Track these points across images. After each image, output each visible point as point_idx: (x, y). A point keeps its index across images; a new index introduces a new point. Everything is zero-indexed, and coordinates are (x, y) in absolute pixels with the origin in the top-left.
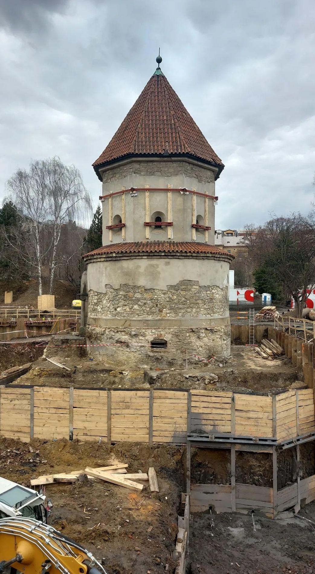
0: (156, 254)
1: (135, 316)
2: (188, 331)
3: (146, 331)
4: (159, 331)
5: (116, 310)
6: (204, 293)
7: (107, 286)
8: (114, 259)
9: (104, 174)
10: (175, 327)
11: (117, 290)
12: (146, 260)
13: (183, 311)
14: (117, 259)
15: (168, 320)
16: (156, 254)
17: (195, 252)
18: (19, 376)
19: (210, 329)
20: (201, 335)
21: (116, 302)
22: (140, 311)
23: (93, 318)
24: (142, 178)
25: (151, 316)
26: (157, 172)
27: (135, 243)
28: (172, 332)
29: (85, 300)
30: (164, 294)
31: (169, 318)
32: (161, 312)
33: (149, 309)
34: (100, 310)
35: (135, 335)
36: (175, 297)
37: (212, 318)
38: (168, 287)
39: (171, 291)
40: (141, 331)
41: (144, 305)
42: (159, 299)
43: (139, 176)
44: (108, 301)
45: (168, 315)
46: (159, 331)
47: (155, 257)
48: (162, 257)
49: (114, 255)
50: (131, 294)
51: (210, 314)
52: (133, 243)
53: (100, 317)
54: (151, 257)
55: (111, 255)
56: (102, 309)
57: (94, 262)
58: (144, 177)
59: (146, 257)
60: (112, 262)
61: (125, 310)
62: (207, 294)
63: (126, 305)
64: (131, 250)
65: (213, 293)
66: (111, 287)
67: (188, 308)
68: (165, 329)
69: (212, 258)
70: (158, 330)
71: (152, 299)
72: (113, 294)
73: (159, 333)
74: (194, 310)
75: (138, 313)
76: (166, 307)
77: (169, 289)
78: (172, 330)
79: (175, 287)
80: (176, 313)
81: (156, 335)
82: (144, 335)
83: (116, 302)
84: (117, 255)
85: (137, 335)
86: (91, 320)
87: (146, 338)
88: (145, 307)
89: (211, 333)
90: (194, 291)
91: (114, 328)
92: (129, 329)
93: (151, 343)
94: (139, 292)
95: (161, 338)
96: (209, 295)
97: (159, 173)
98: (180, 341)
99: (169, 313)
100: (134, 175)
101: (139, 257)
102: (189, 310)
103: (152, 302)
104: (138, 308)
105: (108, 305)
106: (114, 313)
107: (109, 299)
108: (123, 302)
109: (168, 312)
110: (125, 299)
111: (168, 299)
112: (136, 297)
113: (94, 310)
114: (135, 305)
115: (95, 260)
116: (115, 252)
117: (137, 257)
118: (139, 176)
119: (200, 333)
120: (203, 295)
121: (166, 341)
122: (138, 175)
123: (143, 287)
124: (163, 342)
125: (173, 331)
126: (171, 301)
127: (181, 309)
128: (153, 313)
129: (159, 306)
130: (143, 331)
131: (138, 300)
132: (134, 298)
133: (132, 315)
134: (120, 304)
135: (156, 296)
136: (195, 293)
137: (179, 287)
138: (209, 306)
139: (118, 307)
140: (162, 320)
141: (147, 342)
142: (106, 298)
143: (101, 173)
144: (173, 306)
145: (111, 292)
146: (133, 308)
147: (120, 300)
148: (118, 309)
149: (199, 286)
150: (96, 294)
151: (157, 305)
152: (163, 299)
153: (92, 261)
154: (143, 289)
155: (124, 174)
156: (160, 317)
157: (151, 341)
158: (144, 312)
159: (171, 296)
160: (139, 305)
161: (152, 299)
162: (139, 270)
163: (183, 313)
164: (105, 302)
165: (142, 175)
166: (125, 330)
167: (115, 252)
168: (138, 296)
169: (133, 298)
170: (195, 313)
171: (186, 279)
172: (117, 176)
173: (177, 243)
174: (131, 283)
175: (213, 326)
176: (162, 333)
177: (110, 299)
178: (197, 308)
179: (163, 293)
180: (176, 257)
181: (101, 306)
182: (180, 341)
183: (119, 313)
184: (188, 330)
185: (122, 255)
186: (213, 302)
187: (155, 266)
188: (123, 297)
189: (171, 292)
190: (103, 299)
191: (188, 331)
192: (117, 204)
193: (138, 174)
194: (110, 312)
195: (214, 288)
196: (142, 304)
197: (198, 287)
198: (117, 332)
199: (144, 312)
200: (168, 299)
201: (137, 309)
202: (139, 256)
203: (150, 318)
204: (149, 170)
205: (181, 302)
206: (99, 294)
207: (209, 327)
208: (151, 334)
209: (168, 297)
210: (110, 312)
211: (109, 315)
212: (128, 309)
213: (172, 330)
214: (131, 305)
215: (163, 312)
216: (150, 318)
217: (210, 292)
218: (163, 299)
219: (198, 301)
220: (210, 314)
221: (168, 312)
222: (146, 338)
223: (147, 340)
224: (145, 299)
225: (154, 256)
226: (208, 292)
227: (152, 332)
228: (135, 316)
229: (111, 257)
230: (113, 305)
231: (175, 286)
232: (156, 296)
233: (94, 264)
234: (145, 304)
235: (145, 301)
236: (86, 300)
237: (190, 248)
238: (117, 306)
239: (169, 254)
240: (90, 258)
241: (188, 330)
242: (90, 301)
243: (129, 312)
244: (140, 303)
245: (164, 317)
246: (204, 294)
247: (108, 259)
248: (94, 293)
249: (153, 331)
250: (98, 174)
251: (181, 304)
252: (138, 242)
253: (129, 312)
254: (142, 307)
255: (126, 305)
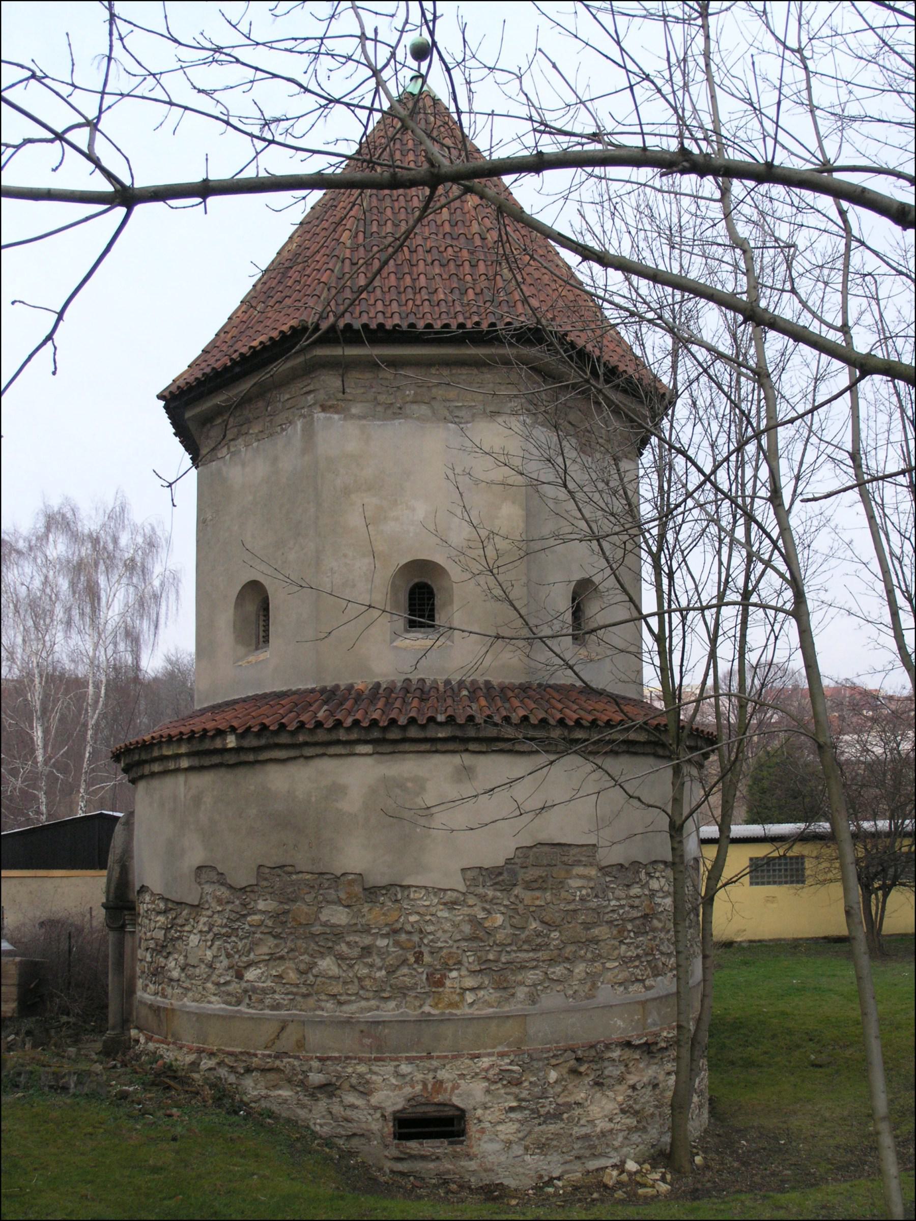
0: (413, 733)
1: (323, 1004)
2: (554, 1062)
3: (375, 1068)
4: (429, 1070)
5: (240, 976)
6: (617, 892)
7: (204, 877)
8: (231, 759)
9: (205, 430)
10: (500, 1049)
11: (243, 890)
12: (369, 761)
13: (532, 976)
14: (244, 757)
15: (472, 1019)
16: (413, 733)
17: (584, 722)
18: (662, 653)
19: (642, 1041)
20: (606, 1073)
21: (240, 945)
22: (345, 983)
23: (151, 1007)
24: (352, 428)
25: (392, 1004)
26: (415, 407)
27: (323, 690)
28: (487, 1070)
29: (123, 926)
30: (451, 905)
31: (474, 1011)
32: (440, 983)
33: (384, 972)
34: (175, 974)
35: (322, 1087)
36: (499, 919)
37: (651, 994)
38: (469, 874)
39: (480, 890)
40: (350, 1070)
41: (361, 957)
42: (430, 928)
43: (340, 419)
44: (210, 936)
45: (470, 997)
46: (429, 1070)
47: (407, 747)
48: (439, 747)
49: (231, 741)
50: (301, 908)
51: (643, 981)
52: (312, 691)
53: (176, 1004)
54: (388, 748)
55: (218, 744)
56: (183, 969)
57: (153, 775)
58: (364, 422)
59: (368, 749)
60: (222, 772)
61: (280, 977)
62: (628, 897)
63: (282, 958)
64: (303, 718)
65: (653, 894)
66: (221, 879)
67: (552, 961)
68: (455, 1057)
69: (648, 749)
70: (427, 1064)
71: (396, 932)
72: (229, 907)
73: (430, 1076)
74: (580, 969)
75: (335, 991)
76: (460, 963)
77: (474, 882)
78: (485, 1062)
79: (500, 874)
80: (502, 986)
81: (419, 1087)
82: (364, 1089)
83: (240, 945)
84: (246, 743)
85: (330, 1089)
86: (144, 1011)
87: (374, 1100)
88: (366, 964)
89: (645, 1056)
90: (580, 888)
91: (231, 1054)
92: (296, 1063)
93: (395, 1119)
94: (339, 902)
95: (439, 1098)
96: (637, 902)
97: (424, 409)
98: (524, 1104)
99: (472, 989)
100: (322, 415)
101: (339, 750)
102: (558, 971)
103: (397, 943)
104: (335, 970)
105: (209, 954)
106: (230, 988)
107: (210, 930)
108: (271, 942)
109: (469, 982)
110: (279, 930)
111: (467, 929)
112: (325, 925)
113: (157, 973)
114: (322, 955)
115: (156, 768)
116: (233, 729)
117: (332, 750)
118: (340, 419)
119: (606, 1064)
120: (613, 903)
121: (463, 1111)
122: (336, 417)
123: (353, 881)
124: (451, 1112)
125: (492, 1066)
126: (481, 934)
127: (523, 968)
128: (402, 992)
129: (427, 958)
130: (362, 1069)
131: (337, 934)
132: (317, 929)
133: (311, 1001)
134: (263, 950)
135: (413, 918)
136: (582, 899)
137: (513, 873)
138: (637, 947)
139: (249, 965)
140: (444, 1020)
141: (378, 1115)
142: (201, 926)
143: (192, 427)
144: (491, 956)
145: (220, 901)
146: (314, 971)
147: (258, 936)
148: (251, 975)
149: (601, 869)
150: (162, 906)
151: (419, 957)
152: (447, 926)
153: (147, 769)
154: (357, 889)
155: (279, 419)
156: (435, 1006)
157: (395, 1113)
158: (362, 988)
159: (481, 915)
160: (340, 957)
161: (396, 932)
162: (339, 805)
163: (535, 985)
164: (194, 939)
165: (353, 417)
166: (278, 1063)
167: (233, 729)
168: (339, 916)
169: (312, 925)
170: (582, 982)
171: (543, 837)
172: (255, 430)
173: (503, 689)
174: (301, 860)
175: (654, 1029)
176: (442, 1074)
177: (215, 929)
178: (593, 960)
179: (445, 904)
180: (501, 746)
181: (181, 959)
182: (524, 1104)
183: (254, 990)
184: (554, 1056)
185: (263, 742)
186: (654, 930)
187: (409, 785)
188: (270, 924)
189: (482, 898)
190: (187, 928)
191: (554, 1062)
192: (525, 873)
193: (337, 412)
194: (218, 984)
195: (656, 870)
196: (356, 952)
197: (593, 872)
198: (248, 1070)
199: (362, 988)
200: (467, 929)
201: (330, 973)
202: (338, 742)
203: (390, 1010)
204: (382, 398)
205: (523, 936)
206: (172, 906)
207: (639, 1037)
208: (394, 1081)
209: (470, 921)
210: (218, 984)
211: (213, 999)
212: (292, 976)
213: (485, 1062)
214: (306, 958)
215: (448, 983)
216: (390, 1010)
217: (642, 887)
218: (447, 926)
219: (596, 931)
220: (643, 981)
221: (469, 982)
222: (374, 1100)
223: (376, 1108)
224: (366, 930)
225: (404, 740)
226: (635, 890)
227: (397, 1074)
228: (323, 1004)
229: (216, 752)
230: (228, 956)
231: (495, 872)
232: (413, 918)
233: (155, 783)
234: (367, 951)
235: (367, 940)
236: (129, 929)
237: (560, 706)
238: (245, 959)
239: (472, 733)
240: (136, 758)
241: (554, 1056)
242: (141, 932)
243: (297, 985)
244: (344, 948)
245: (452, 1005)
246: (618, 899)
247: (207, 761)
248: (153, 902)
249: (405, 1068)
250: (182, 431)
251: (525, 947)
252: (337, 687)
253: (297, 985)
254: (351, 966)
255: (282, 958)
